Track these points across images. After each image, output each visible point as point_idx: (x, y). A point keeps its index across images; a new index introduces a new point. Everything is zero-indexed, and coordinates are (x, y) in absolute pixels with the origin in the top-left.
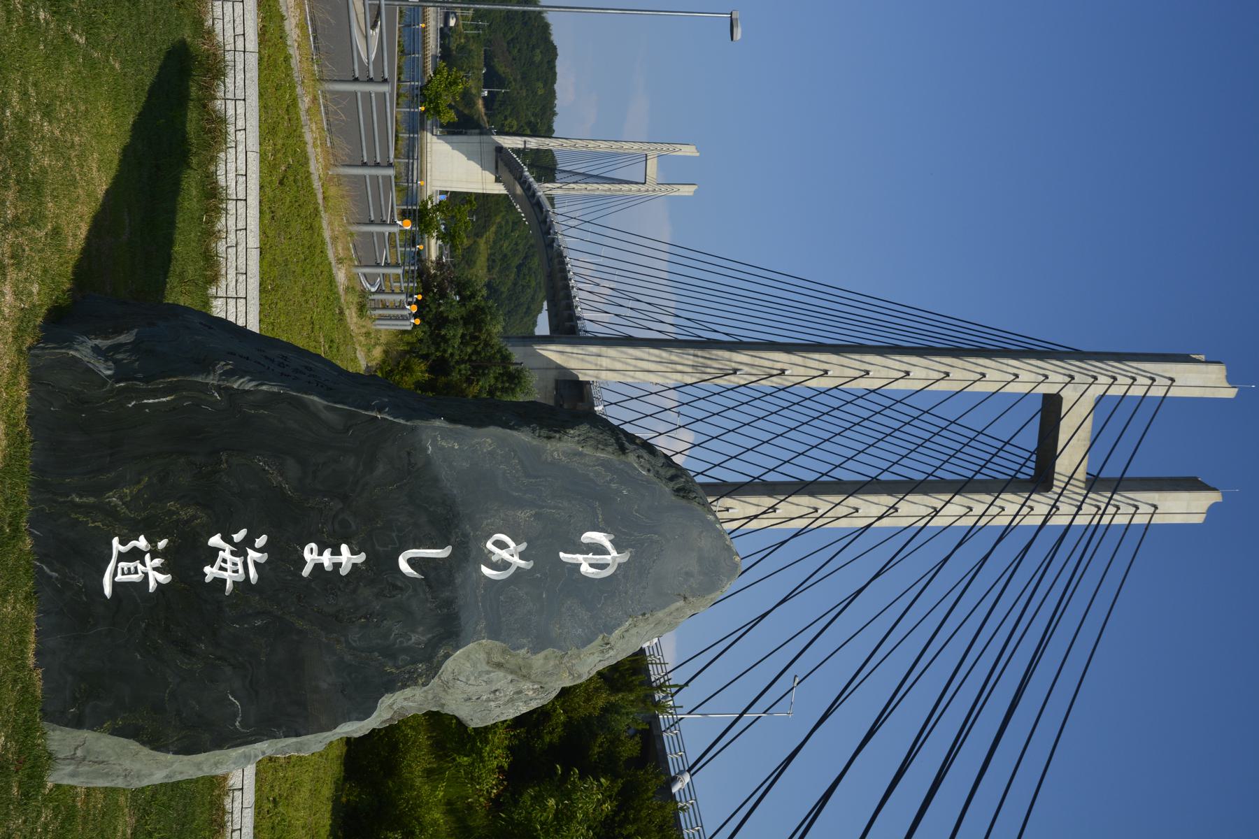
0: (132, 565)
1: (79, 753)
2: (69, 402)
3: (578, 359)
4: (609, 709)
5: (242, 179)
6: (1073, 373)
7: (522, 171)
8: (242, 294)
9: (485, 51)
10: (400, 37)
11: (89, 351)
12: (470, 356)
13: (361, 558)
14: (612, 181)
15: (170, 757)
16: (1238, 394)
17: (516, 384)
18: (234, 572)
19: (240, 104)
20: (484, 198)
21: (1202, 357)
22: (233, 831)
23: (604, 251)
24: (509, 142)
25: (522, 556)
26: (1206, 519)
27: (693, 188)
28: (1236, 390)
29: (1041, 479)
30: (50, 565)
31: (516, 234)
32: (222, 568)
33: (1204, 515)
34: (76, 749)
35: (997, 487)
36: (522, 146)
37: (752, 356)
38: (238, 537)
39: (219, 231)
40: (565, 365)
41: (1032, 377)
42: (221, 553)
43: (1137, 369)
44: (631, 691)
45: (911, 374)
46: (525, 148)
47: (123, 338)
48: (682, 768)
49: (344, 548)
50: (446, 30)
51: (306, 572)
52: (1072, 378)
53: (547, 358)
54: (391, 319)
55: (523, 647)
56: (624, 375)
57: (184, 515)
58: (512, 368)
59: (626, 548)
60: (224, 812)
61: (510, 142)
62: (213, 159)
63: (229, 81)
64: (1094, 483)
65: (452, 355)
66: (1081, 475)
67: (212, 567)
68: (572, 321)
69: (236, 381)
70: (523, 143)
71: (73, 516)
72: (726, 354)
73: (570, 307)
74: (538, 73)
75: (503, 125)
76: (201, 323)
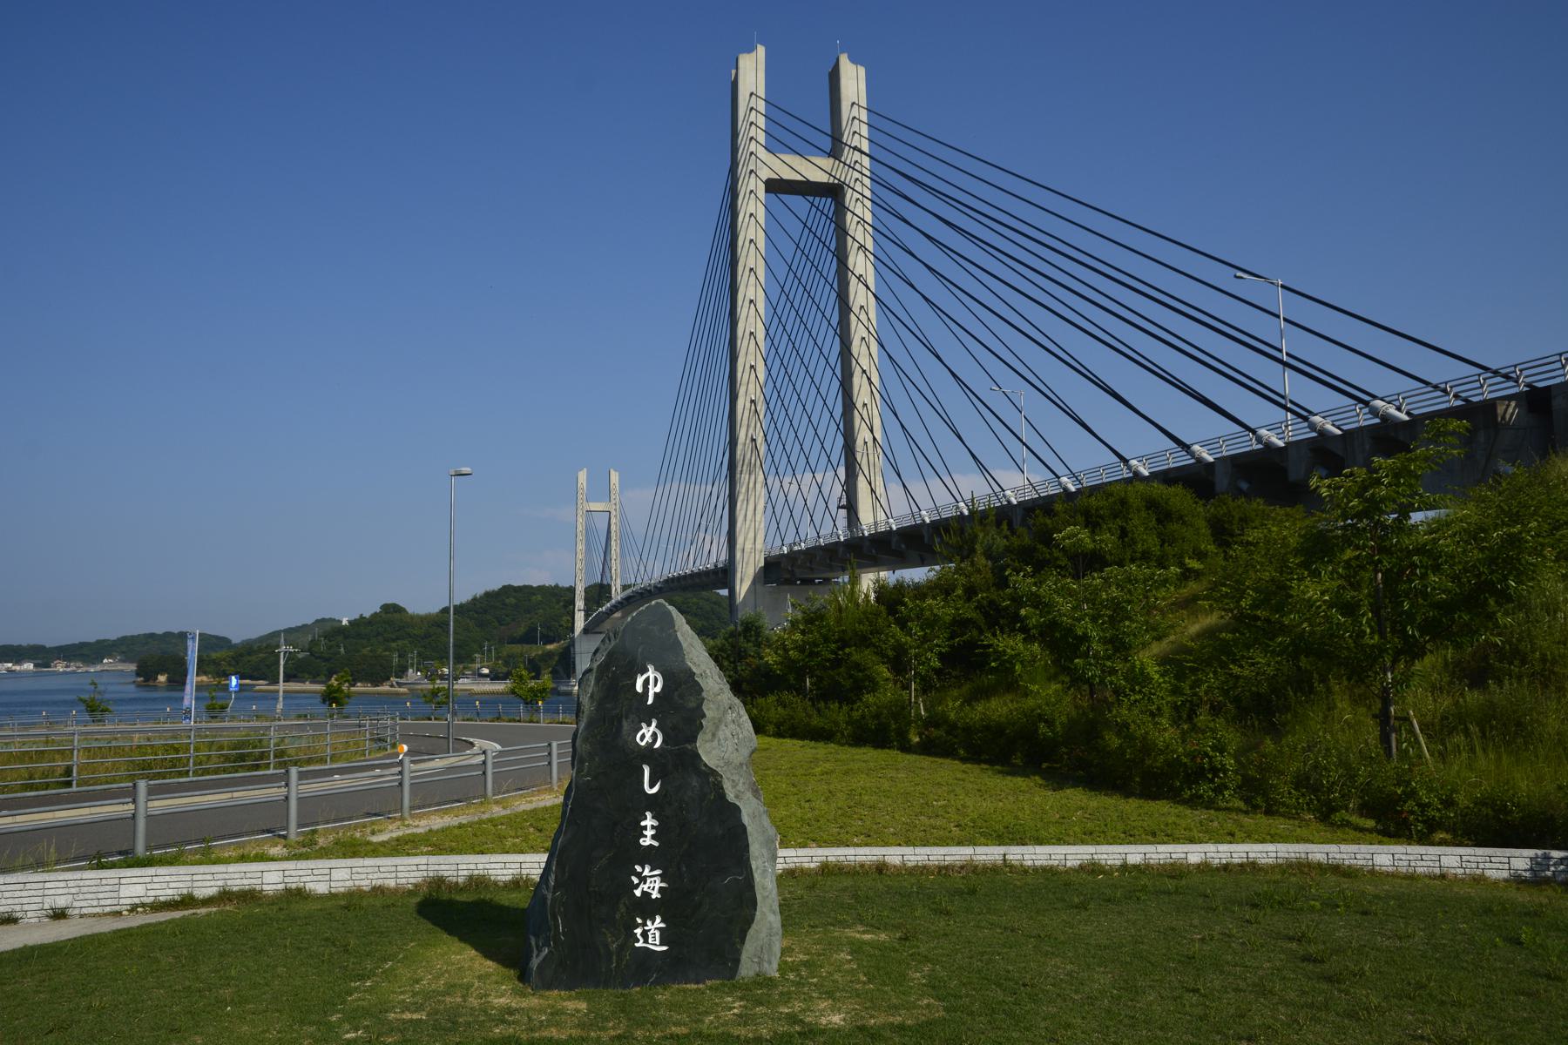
0: (650, 936)
3: (746, 567)
4: (988, 554)
5: (507, 865)
6: (748, 171)
9: (509, 643)
10: (486, 721)
12: (731, 663)
13: (648, 814)
15: (758, 913)
16: (761, 44)
17: (753, 626)
19: (460, 867)
21: (733, 72)
22: (929, 860)
24: (579, 623)
25: (649, 725)
26: (862, 65)
27: (612, 472)
28: (758, 46)
29: (834, 192)
32: (653, 889)
33: (859, 66)
35: (842, 232)
36: (583, 612)
38: (636, 881)
40: (751, 578)
41: (752, 202)
42: (645, 890)
44: (976, 536)
45: (752, 298)
47: (533, 943)
48: (1057, 483)
49: (643, 824)
50: (492, 676)
51: (656, 844)
52: (752, 171)
57: (623, 909)
60: (917, 866)
61: (580, 623)
62: (496, 883)
63: (446, 874)
64: (835, 153)
72: (740, 447)
73: (707, 573)
74: (525, 601)
75: (567, 628)
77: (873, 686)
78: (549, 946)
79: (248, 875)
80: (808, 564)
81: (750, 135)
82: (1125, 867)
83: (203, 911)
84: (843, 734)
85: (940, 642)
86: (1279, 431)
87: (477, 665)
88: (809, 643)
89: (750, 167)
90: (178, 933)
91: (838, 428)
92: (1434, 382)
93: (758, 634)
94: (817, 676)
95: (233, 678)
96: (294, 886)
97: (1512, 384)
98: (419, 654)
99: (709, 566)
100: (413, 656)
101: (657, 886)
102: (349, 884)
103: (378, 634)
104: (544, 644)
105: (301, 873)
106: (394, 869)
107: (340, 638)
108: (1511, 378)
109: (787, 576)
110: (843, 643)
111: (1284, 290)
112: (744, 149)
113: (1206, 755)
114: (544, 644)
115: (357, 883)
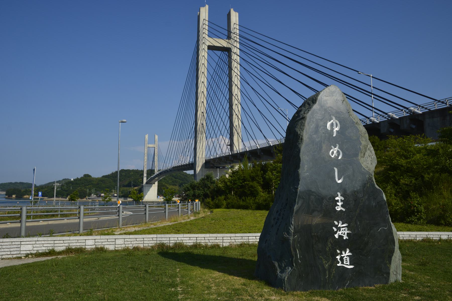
0: (345, 260)
1: (395, 273)
2: (300, 279)
5: (191, 239)
7: (152, 177)
8: (222, 238)
11: (283, 274)
12: (202, 188)
16: (207, 4)
18: (345, 231)
19: (171, 239)
20: (158, 186)
21: (198, 13)
23: (172, 157)
26: (237, 12)
27: (156, 135)
29: (228, 50)
30: (346, 283)
31: (167, 179)
32: (344, 234)
34: (394, 274)
38: (335, 229)
39: (205, 244)
40: (201, 166)
41: (203, 52)
47: (276, 264)
49: (337, 199)
51: (344, 210)
52: (204, 43)
54: (196, 207)
55: (360, 147)
58: (205, 178)
59: (331, 117)
61: (145, 181)
62: (186, 246)
63: (165, 242)
65: (202, 193)
66: (227, 41)
67: (344, 237)
69: (291, 231)
71: (332, 277)
72: (198, 126)
73: (186, 165)
75: (141, 182)
76: (265, 243)
78: (292, 266)
79: (79, 241)
80: (219, 162)
81: (203, 32)
82: (440, 240)
83: (60, 257)
84: (252, 207)
86: (377, 118)
87: (113, 193)
88: (233, 180)
89: (203, 42)
90: (54, 265)
92: (419, 104)
93: (211, 180)
94: (235, 191)
95: (40, 192)
96: (99, 246)
97: (444, 104)
98: (95, 190)
100: (93, 190)
101: (346, 232)
102: (123, 246)
103: (83, 183)
104: (134, 187)
105: (103, 241)
106: (142, 239)
107: (71, 184)
108: (444, 103)
109: (212, 166)
111: (373, 78)
113: (415, 206)
114: (134, 187)
115: (127, 245)
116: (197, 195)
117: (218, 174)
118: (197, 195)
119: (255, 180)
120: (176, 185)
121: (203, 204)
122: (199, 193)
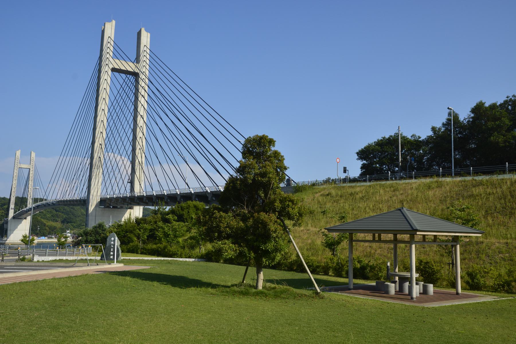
3: (93, 201)
6: (106, 64)
7: (24, 211)
12: (94, 235)
14: (28, 179)
21: (103, 27)
27: (32, 152)
29: (136, 75)
36: (13, 210)
37: (95, 153)
43: (105, 46)
45: (103, 109)
46: (14, 209)
52: (107, 64)
53: (93, 210)
56: (99, 188)
65: (94, 239)
68: (81, 201)
70: (12, 210)
72: (94, 160)
77: (132, 241)
80: (116, 202)
85: (147, 234)
88: (118, 232)
91: (131, 144)
93: (103, 227)
99: (74, 198)
110: (127, 232)
112: (105, 51)
116: (89, 240)
117: (111, 221)
118: (89, 240)
119: (132, 233)
120: (57, 221)
121: (94, 249)
122: (91, 239)
